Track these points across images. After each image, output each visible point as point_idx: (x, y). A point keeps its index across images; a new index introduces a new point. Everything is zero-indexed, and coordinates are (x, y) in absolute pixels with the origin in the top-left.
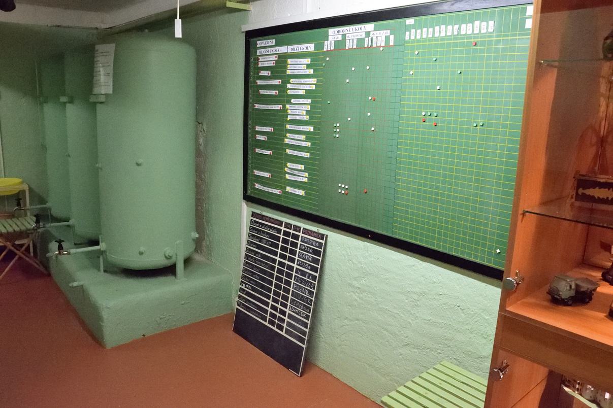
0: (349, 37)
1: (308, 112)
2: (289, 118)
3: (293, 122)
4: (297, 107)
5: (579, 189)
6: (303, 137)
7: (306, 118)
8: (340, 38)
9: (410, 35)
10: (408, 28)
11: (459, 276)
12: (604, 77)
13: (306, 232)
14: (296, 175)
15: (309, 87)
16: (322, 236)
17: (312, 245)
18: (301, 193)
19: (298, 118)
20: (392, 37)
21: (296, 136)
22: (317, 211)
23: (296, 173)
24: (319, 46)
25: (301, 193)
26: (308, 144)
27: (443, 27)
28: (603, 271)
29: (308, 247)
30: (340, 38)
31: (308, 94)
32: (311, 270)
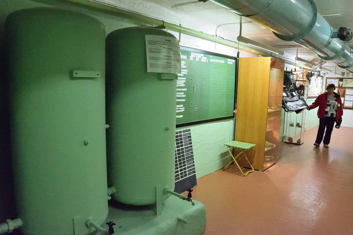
0: (197, 57)
1: (184, 83)
2: (177, 86)
3: (179, 87)
4: (180, 81)
5: (335, 94)
6: (182, 93)
7: (184, 85)
8: (195, 57)
9: (211, 60)
10: (211, 58)
11: (216, 123)
12: (337, 87)
13: (184, 131)
14: (180, 110)
15: (185, 73)
16: (189, 130)
17: (187, 135)
18: (181, 116)
19: (181, 85)
20: (207, 60)
21: (180, 93)
22: (186, 121)
23: (180, 108)
24: (188, 58)
25: (181, 116)
26: (184, 96)
27: (214, 60)
28: (303, 103)
29: (186, 137)
30: (195, 57)
31: (185, 76)
32: (190, 144)
